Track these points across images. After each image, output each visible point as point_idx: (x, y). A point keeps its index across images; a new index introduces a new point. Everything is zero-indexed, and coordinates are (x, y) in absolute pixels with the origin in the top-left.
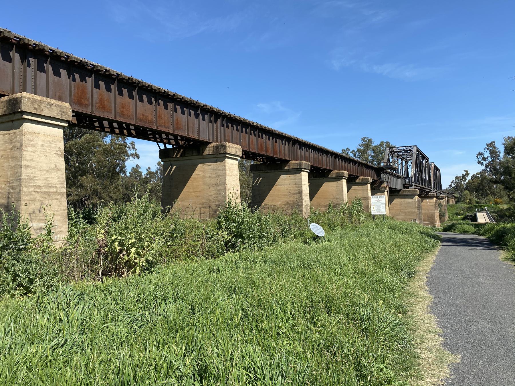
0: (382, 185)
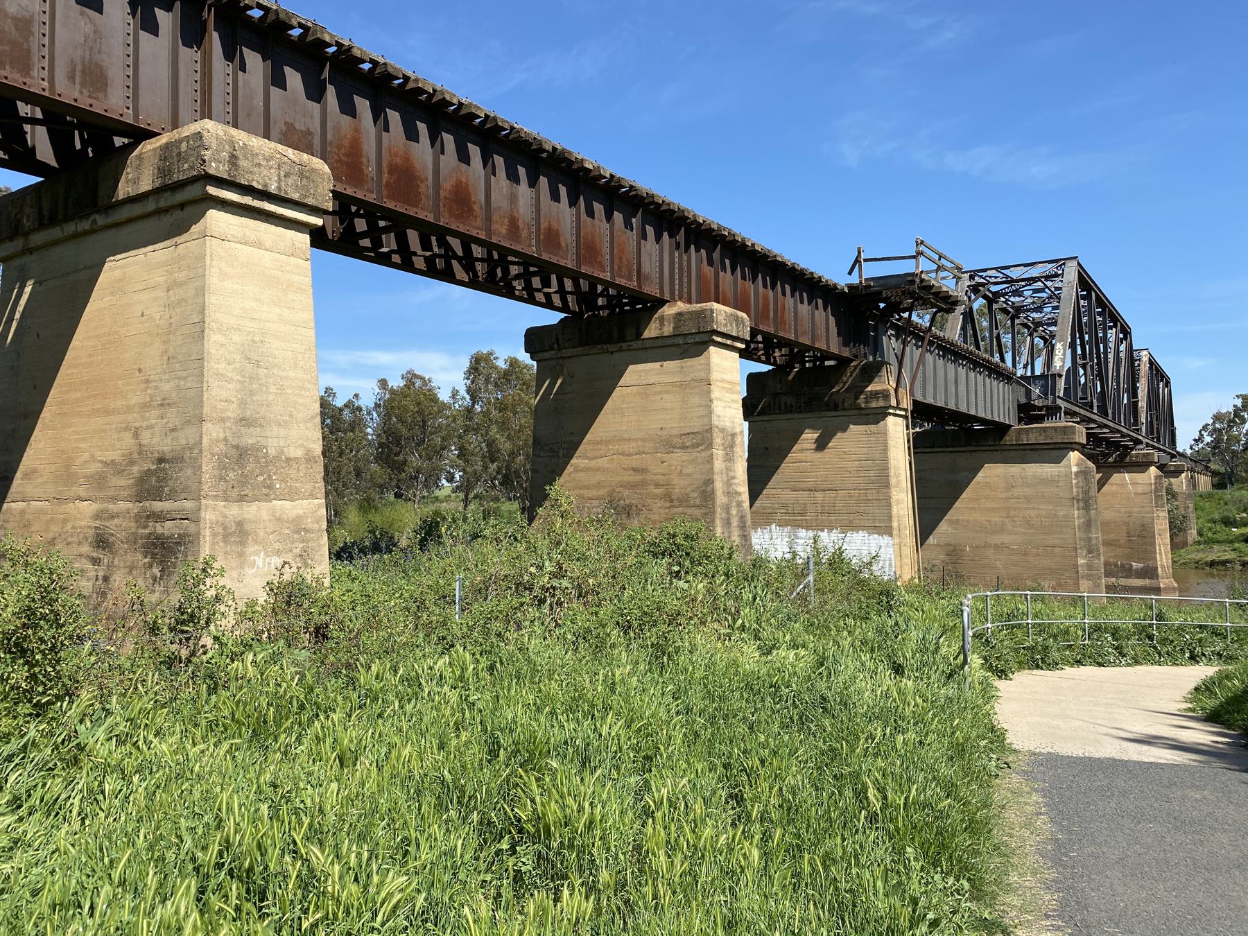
0: (870, 381)
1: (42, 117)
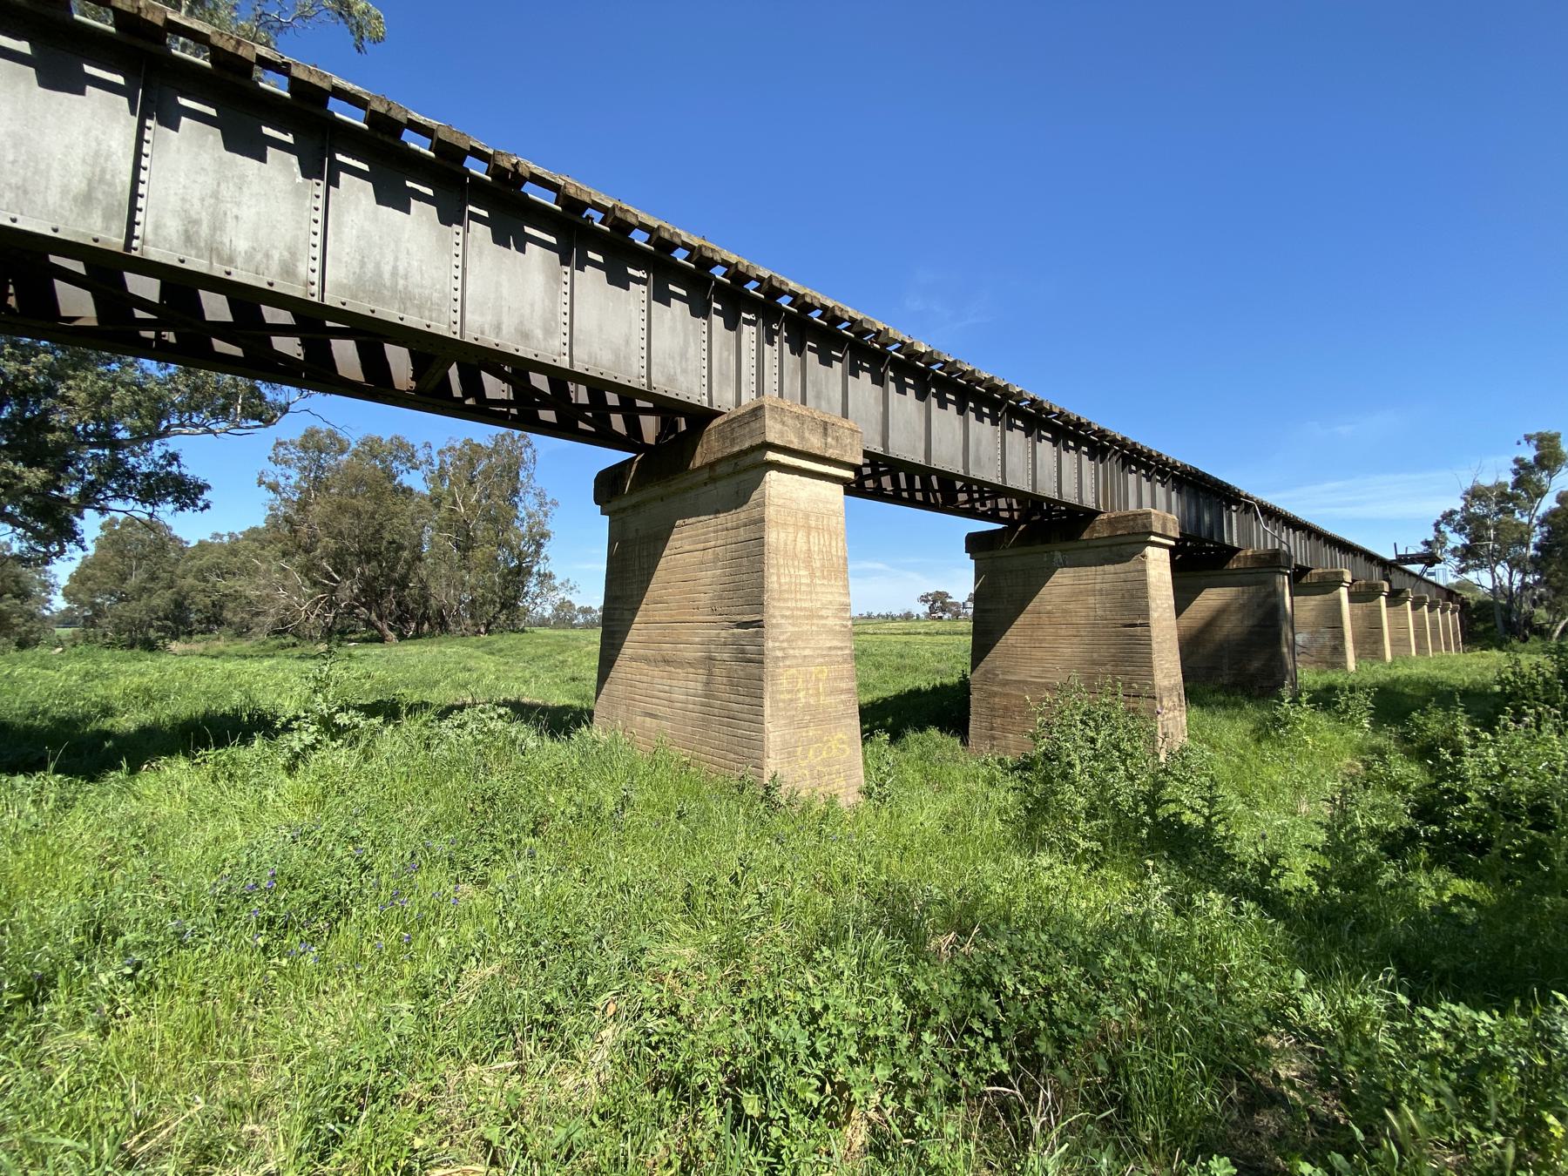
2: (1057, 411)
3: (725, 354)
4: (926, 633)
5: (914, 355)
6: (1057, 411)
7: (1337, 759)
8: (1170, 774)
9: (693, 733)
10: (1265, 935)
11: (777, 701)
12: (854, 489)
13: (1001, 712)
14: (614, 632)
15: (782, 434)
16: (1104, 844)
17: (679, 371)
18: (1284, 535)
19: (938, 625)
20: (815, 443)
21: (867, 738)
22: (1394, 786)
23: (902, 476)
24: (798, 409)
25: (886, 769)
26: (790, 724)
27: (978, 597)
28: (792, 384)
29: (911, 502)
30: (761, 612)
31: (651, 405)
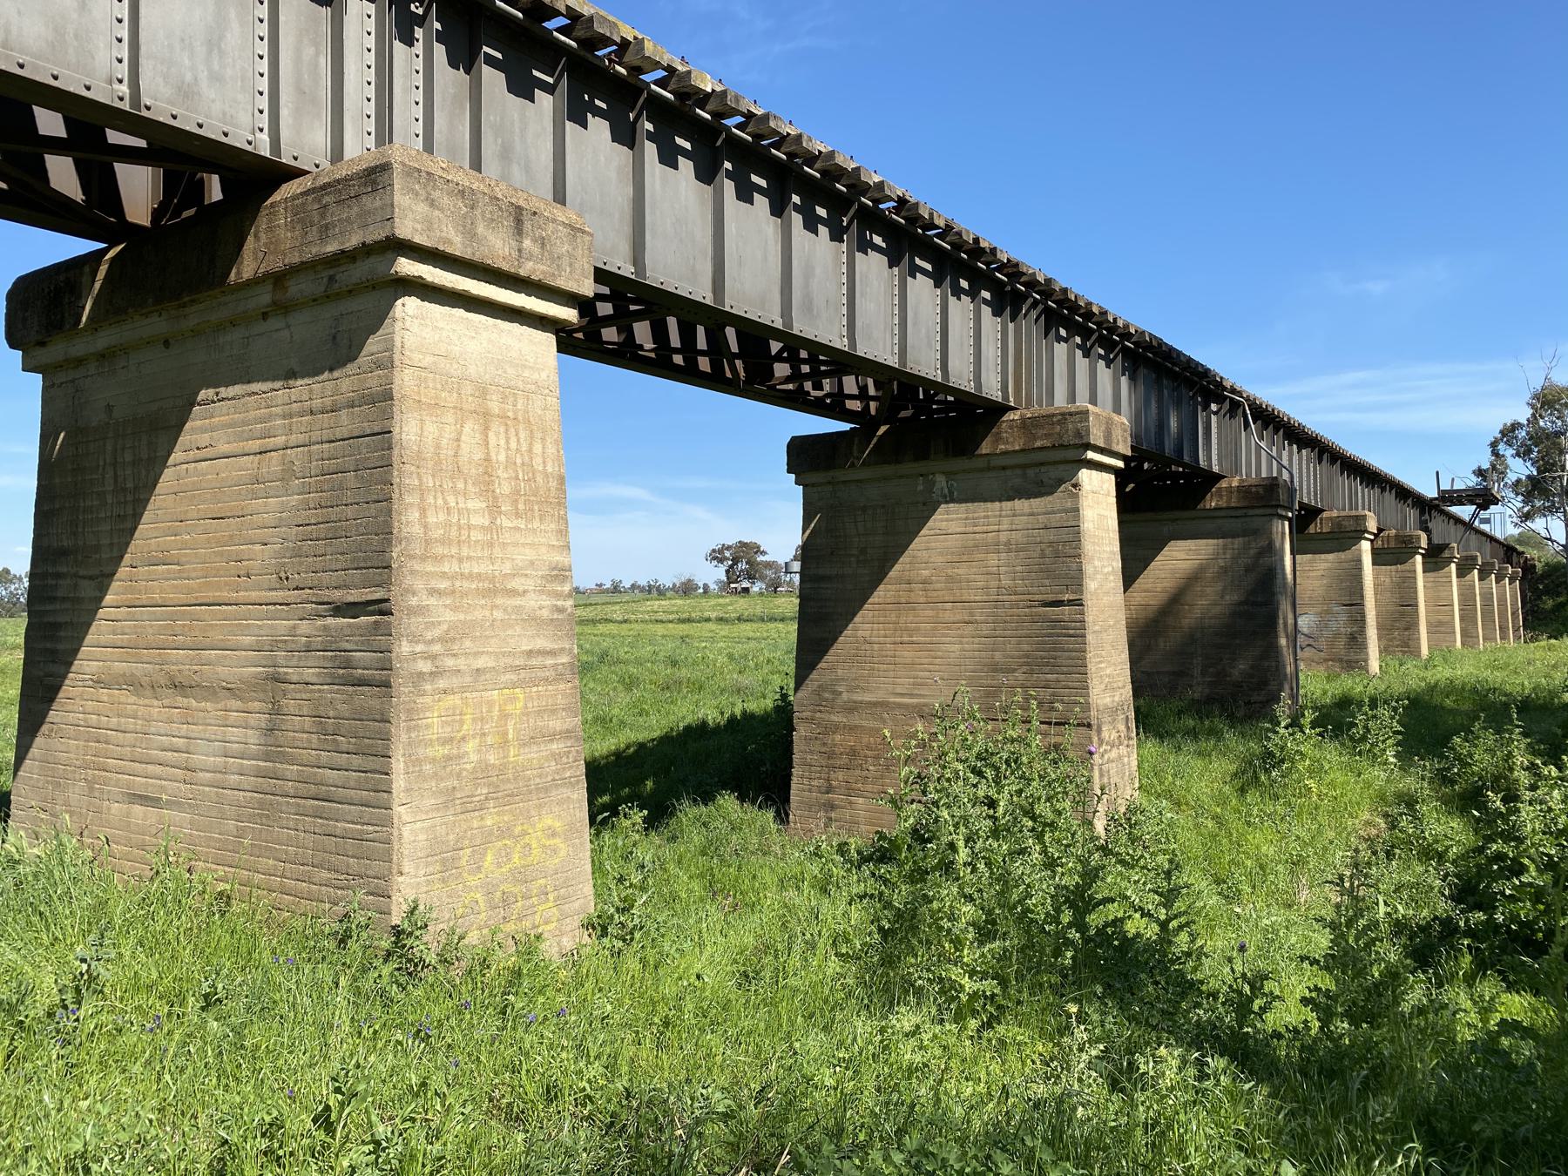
1: (65, 136)
2: (942, 223)
3: (309, 51)
4: (720, 620)
5: (691, 96)
6: (942, 223)
7: (1350, 815)
8: (1111, 852)
9: (240, 834)
10: (1241, 1108)
11: (419, 762)
12: (569, 342)
13: (845, 760)
14: (56, 626)
15: (429, 225)
16: (1003, 982)
17: (203, 75)
18: (1285, 454)
19: (740, 605)
20: (497, 248)
21: (604, 822)
22: (1431, 854)
23: (672, 323)
24: (465, 178)
25: (636, 878)
26: (446, 806)
27: (807, 553)
28: (452, 126)
29: (689, 375)
30: (385, 583)
31: (142, 143)
